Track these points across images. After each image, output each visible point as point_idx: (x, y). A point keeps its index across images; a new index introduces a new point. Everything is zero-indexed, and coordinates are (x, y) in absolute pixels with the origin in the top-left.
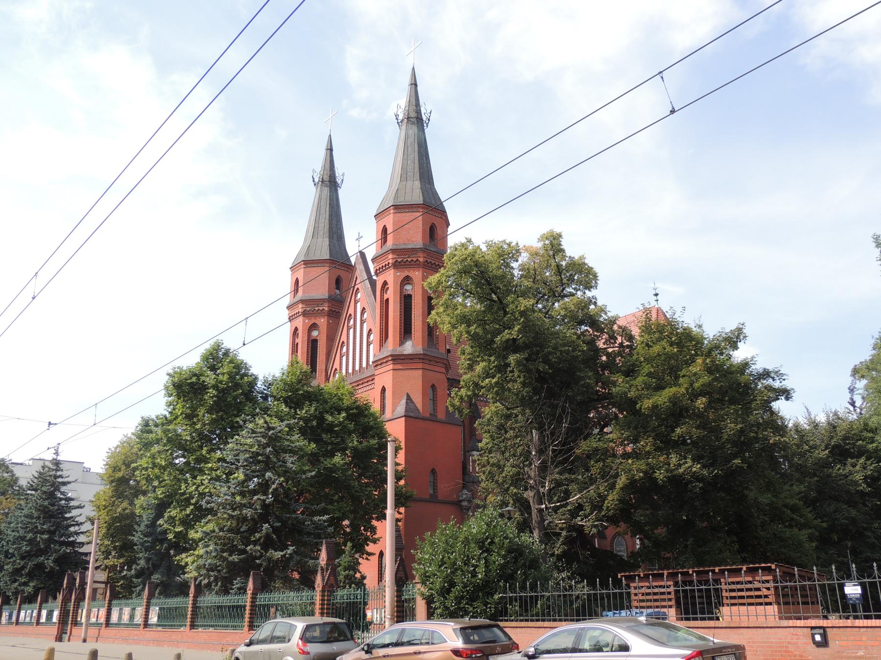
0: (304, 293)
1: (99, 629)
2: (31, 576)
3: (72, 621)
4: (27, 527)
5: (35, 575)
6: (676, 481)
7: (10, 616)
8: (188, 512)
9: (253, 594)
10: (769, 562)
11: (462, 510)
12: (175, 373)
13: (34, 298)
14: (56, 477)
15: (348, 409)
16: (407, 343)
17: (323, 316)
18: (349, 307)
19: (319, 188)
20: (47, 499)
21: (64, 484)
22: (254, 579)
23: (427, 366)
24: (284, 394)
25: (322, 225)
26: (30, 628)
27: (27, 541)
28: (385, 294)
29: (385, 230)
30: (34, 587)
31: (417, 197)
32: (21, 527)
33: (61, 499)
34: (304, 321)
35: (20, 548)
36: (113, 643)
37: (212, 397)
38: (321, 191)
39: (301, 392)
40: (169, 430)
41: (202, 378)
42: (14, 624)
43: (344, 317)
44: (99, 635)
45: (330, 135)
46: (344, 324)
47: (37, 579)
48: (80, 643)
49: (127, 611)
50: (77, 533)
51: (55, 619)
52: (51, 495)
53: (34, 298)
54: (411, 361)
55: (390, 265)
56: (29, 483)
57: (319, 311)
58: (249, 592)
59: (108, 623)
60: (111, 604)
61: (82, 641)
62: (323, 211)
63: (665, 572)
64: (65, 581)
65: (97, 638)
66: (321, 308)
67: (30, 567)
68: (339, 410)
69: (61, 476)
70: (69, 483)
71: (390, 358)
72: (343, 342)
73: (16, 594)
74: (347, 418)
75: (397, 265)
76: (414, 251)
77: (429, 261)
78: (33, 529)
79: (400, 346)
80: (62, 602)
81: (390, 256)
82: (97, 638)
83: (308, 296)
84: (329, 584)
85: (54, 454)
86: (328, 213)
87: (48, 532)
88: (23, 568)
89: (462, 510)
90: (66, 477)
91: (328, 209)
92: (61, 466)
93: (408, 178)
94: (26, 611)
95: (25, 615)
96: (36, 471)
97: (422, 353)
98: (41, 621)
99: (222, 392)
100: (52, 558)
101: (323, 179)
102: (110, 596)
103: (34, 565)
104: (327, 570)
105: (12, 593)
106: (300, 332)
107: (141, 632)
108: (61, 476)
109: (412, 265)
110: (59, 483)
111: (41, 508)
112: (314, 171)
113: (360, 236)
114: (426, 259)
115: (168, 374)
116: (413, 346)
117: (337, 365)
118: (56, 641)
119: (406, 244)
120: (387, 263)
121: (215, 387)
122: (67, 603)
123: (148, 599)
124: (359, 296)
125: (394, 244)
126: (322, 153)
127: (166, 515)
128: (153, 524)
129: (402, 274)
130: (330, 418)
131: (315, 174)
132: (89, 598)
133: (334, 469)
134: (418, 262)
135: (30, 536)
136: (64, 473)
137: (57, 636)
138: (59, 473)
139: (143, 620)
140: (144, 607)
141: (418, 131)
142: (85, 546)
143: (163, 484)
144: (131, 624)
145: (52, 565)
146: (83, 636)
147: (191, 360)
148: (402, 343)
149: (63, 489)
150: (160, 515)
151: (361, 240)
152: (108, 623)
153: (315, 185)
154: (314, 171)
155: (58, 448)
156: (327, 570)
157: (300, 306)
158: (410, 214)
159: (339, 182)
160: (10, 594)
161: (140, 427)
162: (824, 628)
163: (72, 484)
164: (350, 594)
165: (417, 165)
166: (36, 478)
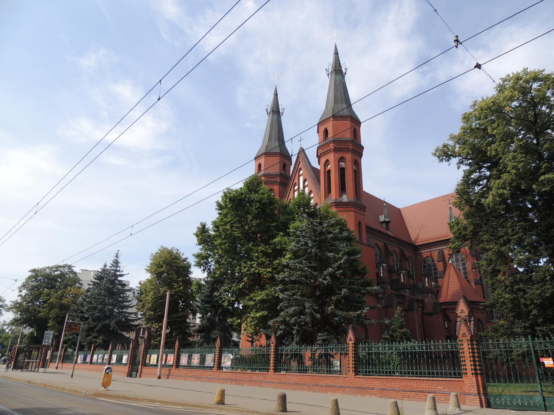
1: (170, 369)
2: (100, 332)
3: (142, 363)
7: (85, 358)
8: (241, 287)
9: (178, 349)
11: (378, 299)
16: (344, 196)
18: (294, 179)
21: (121, 276)
22: (112, 345)
23: (356, 210)
27: (98, 310)
28: (326, 168)
29: (260, 165)
30: (102, 339)
34: (334, 155)
36: (185, 380)
38: (273, 116)
42: (89, 364)
43: (291, 185)
44: (169, 374)
45: (276, 87)
46: (291, 188)
48: (156, 379)
50: (128, 307)
52: (113, 282)
54: (347, 206)
55: (331, 150)
56: (96, 275)
60: (148, 352)
61: (157, 378)
62: (274, 127)
66: (275, 180)
67: (100, 327)
69: (119, 271)
71: (334, 204)
75: (336, 150)
76: (346, 142)
77: (355, 149)
79: (339, 197)
81: (332, 145)
85: (116, 257)
88: (95, 327)
89: (378, 299)
90: (121, 272)
91: (277, 126)
94: (98, 356)
95: (98, 358)
97: (354, 201)
98: (112, 362)
102: (179, 345)
104: (470, 321)
105: (87, 343)
108: (119, 271)
109: (345, 150)
113: (302, 139)
114: (353, 147)
116: (348, 197)
118: (127, 377)
120: (329, 149)
122: (136, 350)
123: (220, 348)
124: (301, 172)
126: (271, 97)
132: (163, 346)
134: (349, 149)
136: (121, 269)
137: (128, 373)
138: (118, 269)
139: (90, 360)
141: (278, 117)
144: (189, 366)
146: (158, 374)
148: (341, 196)
149: (120, 278)
151: (302, 141)
155: (118, 253)
156: (147, 341)
158: (343, 121)
160: (86, 344)
164: (297, 349)
166: (100, 272)
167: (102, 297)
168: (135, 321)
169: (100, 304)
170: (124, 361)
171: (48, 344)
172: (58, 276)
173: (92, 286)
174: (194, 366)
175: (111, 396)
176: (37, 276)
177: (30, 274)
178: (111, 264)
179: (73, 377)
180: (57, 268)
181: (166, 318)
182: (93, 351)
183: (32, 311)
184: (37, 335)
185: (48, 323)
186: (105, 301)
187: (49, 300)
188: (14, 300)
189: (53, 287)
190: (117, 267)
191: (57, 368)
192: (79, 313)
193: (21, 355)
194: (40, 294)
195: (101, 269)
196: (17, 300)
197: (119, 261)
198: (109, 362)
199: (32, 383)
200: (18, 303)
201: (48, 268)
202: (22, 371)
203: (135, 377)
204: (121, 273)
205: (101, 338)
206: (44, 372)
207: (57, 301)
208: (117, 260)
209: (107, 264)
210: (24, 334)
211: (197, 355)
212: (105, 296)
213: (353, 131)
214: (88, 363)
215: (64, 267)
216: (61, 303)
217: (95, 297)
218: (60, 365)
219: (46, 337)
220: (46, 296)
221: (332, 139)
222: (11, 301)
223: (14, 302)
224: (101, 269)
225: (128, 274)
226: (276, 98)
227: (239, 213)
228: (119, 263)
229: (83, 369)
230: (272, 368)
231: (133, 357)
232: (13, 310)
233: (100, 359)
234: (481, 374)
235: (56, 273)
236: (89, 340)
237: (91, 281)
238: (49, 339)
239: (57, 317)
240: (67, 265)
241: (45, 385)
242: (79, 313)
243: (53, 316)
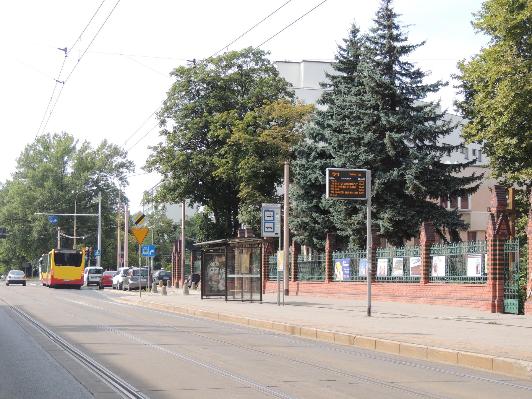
5: (386, 202)
7: (354, 268)
13: (79, 61)
22: (329, 240)
26: (411, 288)
27: (365, 145)
30: (390, 220)
32: (349, 124)
44: (298, 289)
47: (391, 208)
53: (79, 61)
56: (337, 58)
58: (327, 251)
60: (332, 256)
65: (297, 292)
80: (495, 241)
82: (297, 292)
84: (500, 233)
90: (403, 40)
96: (344, 40)
98: (434, 275)
102: (330, 247)
103: (383, 184)
104: (498, 217)
105: (353, 230)
107: (422, 287)
118: (493, 311)
137: (493, 301)
140: (423, 256)
142: (454, 153)
149: (403, 58)
156: (498, 217)
163: (418, 48)
166: (344, 50)
167: (368, 112)
168: (462, 169)
169: (367, 129)
171: (273, 235)
172: (231, 79)
173: (332, 88)
177: (174, 79)
178: (377, 21)
179: (372, 314)
183: (198, 164)
184: (217, 220)
185: (238, 192)
186: (379, 118)
187: (228, 136)
188: (155, 144)
189: (227, 107)
190: (390, 27)
191: (287, 292)
192: (315, 158)
193: (212, 264)
195: (346, 41)
196: (162, 143)
197: (394, 11)
198: (426, 274)
199: (300, 334)
200: (164, 150)
202: (226, 300)
203: (516, 311)
204: (404, 44)
205: (387, 216)
206: (279, 303)
207: (248, 137)
208: (387, 9)
209: (357, 27)
210: (174, 224)
211: (441, 258)
212: (375, 107)
214: (365, 278)
215: (244, 54)
217: (352, 113)
218: (293, 286)
219: (267, 219)
220: (220, 129)
222: (150, 148)
223: (155, 148)
224: (346, 41)
225: (423, 43)
228: (394, 16)
229: (355, 294)
230: (327, 276)
232: (157, 166)
233: (397, 268)
234: (500, 279)
236: (358, 223)
237: (328, 75)
238: (273, 222)
239: (255, 175)
240: (250, 50)
241: (352, 340)
242: (315, 158)
243: (246, 174)
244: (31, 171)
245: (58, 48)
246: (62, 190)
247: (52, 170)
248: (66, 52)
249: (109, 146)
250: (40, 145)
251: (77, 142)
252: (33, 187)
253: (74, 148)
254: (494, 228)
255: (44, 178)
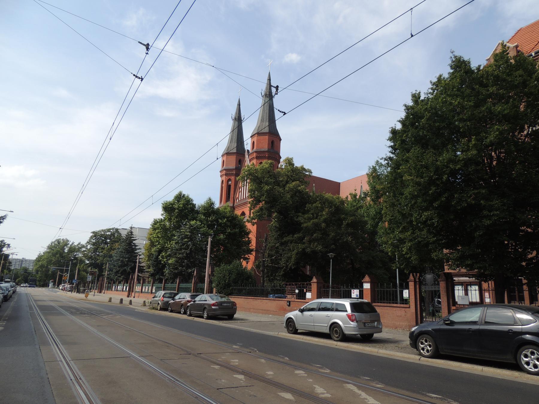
0: (226, 166)
4: (121, 256)
6: (314, 252)
10: (297, 282)
12: (165, 203)
14: (131, 237)
15: (228, 218)
17: (233, 176)
19: (264, 98)
20: (128, 246)
21: (134, 240)
24: (203, 211)
25: (234, 138)
31: (267, 130)
33: (133, 246)
34: (226, 178)
35: (118, 263)
37: (177, 213)
38: (235, 122)
39: (210, 211)
40: (161, 224)
41: (174, 206)
49: (147, 287)
51: (127, 290)
57: (230, 174)
59: (142, 292)
63: (288, 283)
64: (130, 276)
66: (232, 173)
68: (224, 217)
69: (133, 237)
70: (136, 240)
72: (240, 187)
73: (117, 280)
74: (228, 220)
78: (123, 256)
83: (227, 168)
86: (237, 133)
87: (128, 258)
88: (119, 271)
92: (133, 233)
93: (3, 294)
99: (181, 211)
100: (129, 268)
101: (235, 118)
103: (123, 270)
106: (224, 182)
108: (133, 237)
110: (132, 239)
111: (126, 249)
112: (232, 115)
114: (268, 155)
115: (162, 204)
117: (237, 196)
119: (261, 149)
121: (178, 209)
125: (256, 149)
127: (161, 255)
128: (157, 257)
129: (259, 161)
130: (220, 221)
131: (263, 92)
133: (220, 240)
135: (121, 259)
138: (132, 236)
143: (160, 243)
145: (129, 270)
147: (170, 198)
149: (134, 242)
150: (159, 255)
152: (142, 292)
153: (262, 96)
154: (232, 115)
156: (211, 275)
157: (224, 171)
159: (242, 119)
161: (153, 222)
162: (290, 301)
163: (137, 240)
165: (268, 116)
170: (487, 300)
171: (89, 280)
174: (153, 293)
175: (88, 300)
176: (95, 236)
177: (92, 234)
180: (109, 230)
181: (209, 259)
182: (142, 284)
194: (98, 247)
201: (103, 230)
213: (271, 143)
214: (150, 292)
216: (110, 254)
221: (255, 150)
226: (269, 82)
227: (176, 210)
231: (196, 288)
235: (108, 233)
238: (90, 278)
244: (52, 251)
245: (139, 42)
246: (62, 258)
247: (59, 251)
248: (148, 49)
249: (81, 244)
250: (57, 242)
251: (70, 242)
252: (52, 256)
253: (69, 244)
254: (209, 280)
255: (56, 254)
